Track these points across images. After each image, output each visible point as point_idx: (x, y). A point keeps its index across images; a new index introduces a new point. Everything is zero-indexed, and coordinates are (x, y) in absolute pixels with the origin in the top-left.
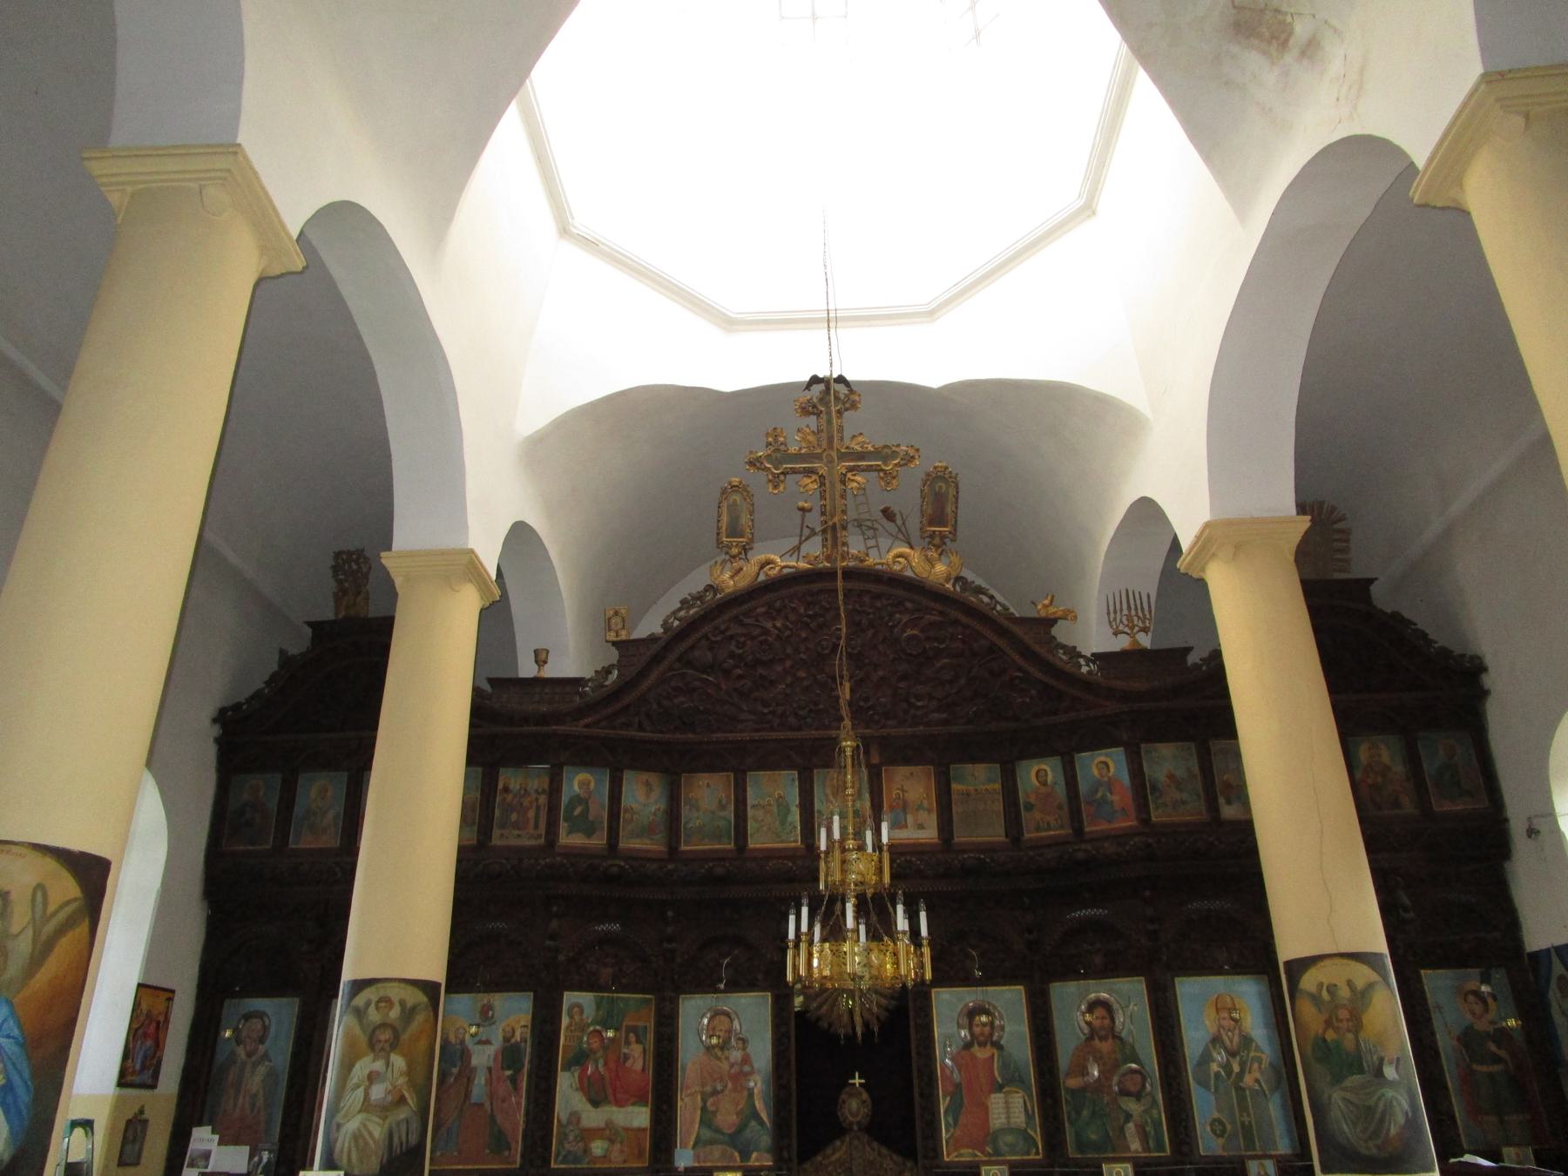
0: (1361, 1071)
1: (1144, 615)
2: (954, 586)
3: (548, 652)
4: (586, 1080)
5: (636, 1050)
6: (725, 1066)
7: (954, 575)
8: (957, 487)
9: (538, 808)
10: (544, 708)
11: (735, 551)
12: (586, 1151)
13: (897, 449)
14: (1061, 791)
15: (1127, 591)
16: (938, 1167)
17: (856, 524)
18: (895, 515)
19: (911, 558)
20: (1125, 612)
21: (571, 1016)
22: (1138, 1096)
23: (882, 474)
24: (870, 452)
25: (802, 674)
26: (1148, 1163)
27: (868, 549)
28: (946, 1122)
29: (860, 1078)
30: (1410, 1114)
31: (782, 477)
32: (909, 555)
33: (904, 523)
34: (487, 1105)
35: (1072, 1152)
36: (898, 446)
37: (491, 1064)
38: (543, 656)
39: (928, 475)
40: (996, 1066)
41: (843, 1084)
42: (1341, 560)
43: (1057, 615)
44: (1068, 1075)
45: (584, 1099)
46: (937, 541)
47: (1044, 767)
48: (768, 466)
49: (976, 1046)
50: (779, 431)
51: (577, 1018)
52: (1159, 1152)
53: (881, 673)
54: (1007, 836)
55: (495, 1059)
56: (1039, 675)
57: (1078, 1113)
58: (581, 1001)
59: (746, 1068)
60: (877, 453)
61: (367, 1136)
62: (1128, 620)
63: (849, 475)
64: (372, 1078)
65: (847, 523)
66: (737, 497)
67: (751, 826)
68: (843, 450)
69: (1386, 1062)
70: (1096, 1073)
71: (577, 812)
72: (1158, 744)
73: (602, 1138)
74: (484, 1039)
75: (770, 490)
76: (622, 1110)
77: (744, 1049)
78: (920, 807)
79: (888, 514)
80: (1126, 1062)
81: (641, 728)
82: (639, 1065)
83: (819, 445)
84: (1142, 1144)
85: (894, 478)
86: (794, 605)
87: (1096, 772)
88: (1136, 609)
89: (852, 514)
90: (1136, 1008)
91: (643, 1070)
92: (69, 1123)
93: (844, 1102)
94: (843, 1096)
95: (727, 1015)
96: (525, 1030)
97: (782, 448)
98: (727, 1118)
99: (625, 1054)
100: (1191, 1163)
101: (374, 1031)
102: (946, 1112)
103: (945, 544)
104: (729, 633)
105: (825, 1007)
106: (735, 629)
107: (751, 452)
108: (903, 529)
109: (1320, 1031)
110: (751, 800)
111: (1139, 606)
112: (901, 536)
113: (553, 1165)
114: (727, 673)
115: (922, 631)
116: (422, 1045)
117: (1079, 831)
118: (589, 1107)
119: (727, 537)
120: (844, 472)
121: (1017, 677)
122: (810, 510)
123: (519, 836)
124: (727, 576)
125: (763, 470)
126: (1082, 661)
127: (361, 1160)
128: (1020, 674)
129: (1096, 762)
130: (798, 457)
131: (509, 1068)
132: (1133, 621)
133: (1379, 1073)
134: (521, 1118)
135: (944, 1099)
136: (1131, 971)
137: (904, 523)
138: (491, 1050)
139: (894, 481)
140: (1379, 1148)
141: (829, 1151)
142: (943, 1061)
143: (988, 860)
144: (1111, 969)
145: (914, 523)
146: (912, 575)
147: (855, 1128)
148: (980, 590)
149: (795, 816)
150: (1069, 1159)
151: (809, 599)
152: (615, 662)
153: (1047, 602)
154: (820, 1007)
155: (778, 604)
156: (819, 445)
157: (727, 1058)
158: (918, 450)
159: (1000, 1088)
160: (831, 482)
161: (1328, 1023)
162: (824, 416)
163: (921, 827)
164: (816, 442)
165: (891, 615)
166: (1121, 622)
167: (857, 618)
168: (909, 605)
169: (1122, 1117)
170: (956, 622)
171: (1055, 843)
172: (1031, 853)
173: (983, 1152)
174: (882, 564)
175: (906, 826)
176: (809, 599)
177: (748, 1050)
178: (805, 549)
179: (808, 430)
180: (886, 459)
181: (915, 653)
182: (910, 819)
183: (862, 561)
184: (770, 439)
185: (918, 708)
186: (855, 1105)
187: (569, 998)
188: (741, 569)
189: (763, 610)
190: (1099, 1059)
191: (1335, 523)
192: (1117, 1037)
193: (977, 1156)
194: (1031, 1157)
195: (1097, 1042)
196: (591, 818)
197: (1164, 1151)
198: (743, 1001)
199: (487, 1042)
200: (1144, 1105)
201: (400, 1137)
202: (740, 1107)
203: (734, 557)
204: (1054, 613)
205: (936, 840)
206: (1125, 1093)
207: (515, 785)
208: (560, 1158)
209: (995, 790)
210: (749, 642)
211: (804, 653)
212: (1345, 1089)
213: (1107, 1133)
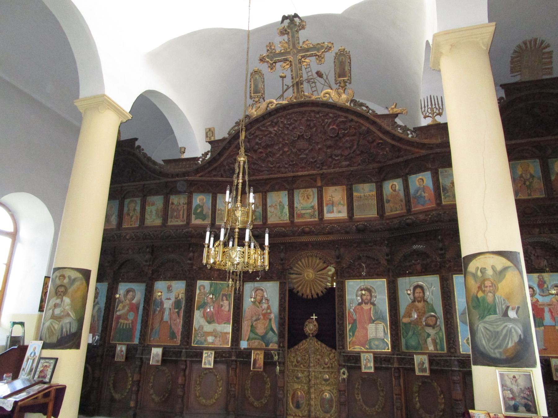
0: (495, 313)
1: (439, 107)
2: (350, 104)
3: (185, 148)
4: (206, 314)
5: (226, 303)
6: (260, 309)
7: (350, 98)
8: (350, 58)
9: (184, 210)
10: (184, 170)
11: (257, 99)
12: (206, 340)
13: (323, 45)
14: (402, 193)
15: (431, 96)
16: (344, 353)
17: (307, 81)
18: (323, 75)
19: (331, 94)
20: (430, 106)
21: (200, 290)
22: (433, 327)
23: (317, 57)
24: (311, 48)
25: (286, 149)
26: (436, 355)
27: (313, 92)
28: (350, 335)
29: (313, 316)
30: (522, 337)
31: (274, 64)
32: (330, 92)
33: (327, 78)
34: (169, 322)
35: (404, 349)
36: (324, 43)
37: (171, 307)
38: (183, 150)
39: (336, 54)
40: (372, 312)
41: (308, 317)
42: (548, 68)
43: (397, 112)
44: (404, 317)
45: (205, 321)
46: (342, 84)
47: (394, 183)
48: (268, 60)
49: (364, 304)
50: (271, 44)
51: (202, 290)
52: (441, 351)
53: (319, 146)
54: (378, 215)
55: (172, 305)
56: (389, 140)
57: (407, 334)
58: (204, 284)
59: (269, 311)
60: (315, 48)
61: (53, 329)
62: (431, 110)
63: (303, 60)
64: (56, 306)
65: (303, 81)
66: (257, 76)
67: (269, 214)
68: (299, 48)
69: (510, 308)
70: (416, 316)
71: (199, 211)
72: (448, 169)
73: (212, 336)
74: (168, 298)
75: (269, 71)
76: (220, 325)
77: (268, 303)
78: (340, 203)
79: (319, 74)
80: (429, 312)
81: (222, 176)
82: (227, 309)
83: (289, 48)
84: (434, 347)
85: (323, 58)
86: (282, 120)
87: (417, 183)
88: (435, 104)
89: (305, 76)
90: (434, 289)
91: (229, 311)
92: (12, 323)
93: (307, 325)
94: (307, 323)
95: (262, 290)
96: (182, 294)
97: (274, 51)
98: (261, 330)
99: (221, 305)
100: (455, 357)
101: (58, 287)
102: (350, 331)
103: (346, 85)
104: (255, 135)
105: (300, 287)
106: (258, 133)
107: (261, 55)
108: (327, 81)
109: (476, 292)
110: (269, 204)
111: (436, 103)
112: (326, 84)
113: (192, 345)
114: (255, 151)
115: (337, 126)
116: (80, 294)
117: (409, 210)
118: (207, 324)
119: (254, 94)
120: (300, 58)
121: (380, 143)
122: (285, 77)
123: (177, 221)
124: (254, 110)
125: (266, 62)
126: (409, 132)
127: (49, 337)
128: (381, 141)
129: (418, 179)
130: (281, 54)
131: (177, 309)
132: (433, 111)
133: (505, 314)
134: (180, 327)
135: (349, 326)
136: (433, 273)
137: (327, 78)
138: (171, 302)
139: (323, 60)
140: (500, 353)
141: (301, 344)
142: (349, 310)
143: (368, 225)
144: (425, 271)
145: (332, 79)
146: (332, 101)
147: (311, 335)
148: (362, 105)
149: (286, 210)
150: (232, 348)
151: (288, 117)
152: (210, 150)
153: (393, 107)
154: (298, 287)
155: (275, 120)
156: (289, 48)
157: (261, 307)
158: (333, 44)
159: (374, 321)
160: (295, 64)
161: (480, 288)
162: (290, 34)
163: (340, 212)
164: (288, 47)
165: (323, 121)
166: (427, 111)
167: (308, 123)
168: (331, 115)
169: (426, 335)
170: (352, 120)
171: (401, 216)
172: (388, 221)
173: (364, 347)
174: (319, 98)
175: (333, 212)
176: (288, 117)
177: (269, 304)
178: (286, 95)
179: (284, 42)
180: (318, 50)
181: (333, 136)
182: (335, 209)
183: (310, 97)
184: (268, 48)
185: (336, 160)
186: (311, 327)
187: (200, 283)
188: (259, 107)
189: (269, 123)
190: (417, 310)
191: (544, 48)
192: (425, 301)
193: (362, 349)
194: (385, 351)
195: (416, 303)
196: (204, 213)
197: (443, 350)
198: (268, 285)
199: (170, 299)
200: (436, 330)
201: (66, 328)
202: (266, 326)
203: (257, 102)
204: (396, 111)
205: (346, 218)
206: (428, 325)
207: (175, 202)
208: (195, 342)
209: (373, 195)
210: (264, 138)
211: (287, 140)
212: (485, 322)
213: (419, 341)
